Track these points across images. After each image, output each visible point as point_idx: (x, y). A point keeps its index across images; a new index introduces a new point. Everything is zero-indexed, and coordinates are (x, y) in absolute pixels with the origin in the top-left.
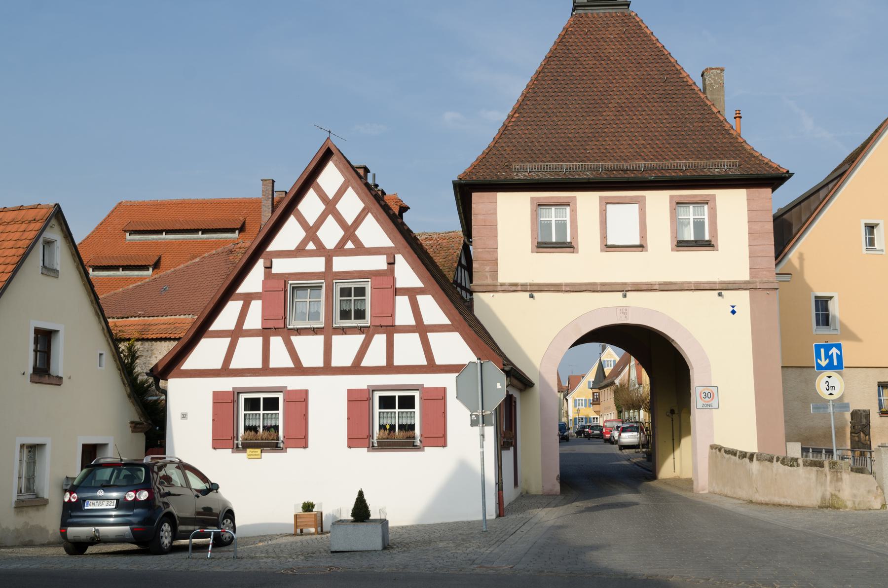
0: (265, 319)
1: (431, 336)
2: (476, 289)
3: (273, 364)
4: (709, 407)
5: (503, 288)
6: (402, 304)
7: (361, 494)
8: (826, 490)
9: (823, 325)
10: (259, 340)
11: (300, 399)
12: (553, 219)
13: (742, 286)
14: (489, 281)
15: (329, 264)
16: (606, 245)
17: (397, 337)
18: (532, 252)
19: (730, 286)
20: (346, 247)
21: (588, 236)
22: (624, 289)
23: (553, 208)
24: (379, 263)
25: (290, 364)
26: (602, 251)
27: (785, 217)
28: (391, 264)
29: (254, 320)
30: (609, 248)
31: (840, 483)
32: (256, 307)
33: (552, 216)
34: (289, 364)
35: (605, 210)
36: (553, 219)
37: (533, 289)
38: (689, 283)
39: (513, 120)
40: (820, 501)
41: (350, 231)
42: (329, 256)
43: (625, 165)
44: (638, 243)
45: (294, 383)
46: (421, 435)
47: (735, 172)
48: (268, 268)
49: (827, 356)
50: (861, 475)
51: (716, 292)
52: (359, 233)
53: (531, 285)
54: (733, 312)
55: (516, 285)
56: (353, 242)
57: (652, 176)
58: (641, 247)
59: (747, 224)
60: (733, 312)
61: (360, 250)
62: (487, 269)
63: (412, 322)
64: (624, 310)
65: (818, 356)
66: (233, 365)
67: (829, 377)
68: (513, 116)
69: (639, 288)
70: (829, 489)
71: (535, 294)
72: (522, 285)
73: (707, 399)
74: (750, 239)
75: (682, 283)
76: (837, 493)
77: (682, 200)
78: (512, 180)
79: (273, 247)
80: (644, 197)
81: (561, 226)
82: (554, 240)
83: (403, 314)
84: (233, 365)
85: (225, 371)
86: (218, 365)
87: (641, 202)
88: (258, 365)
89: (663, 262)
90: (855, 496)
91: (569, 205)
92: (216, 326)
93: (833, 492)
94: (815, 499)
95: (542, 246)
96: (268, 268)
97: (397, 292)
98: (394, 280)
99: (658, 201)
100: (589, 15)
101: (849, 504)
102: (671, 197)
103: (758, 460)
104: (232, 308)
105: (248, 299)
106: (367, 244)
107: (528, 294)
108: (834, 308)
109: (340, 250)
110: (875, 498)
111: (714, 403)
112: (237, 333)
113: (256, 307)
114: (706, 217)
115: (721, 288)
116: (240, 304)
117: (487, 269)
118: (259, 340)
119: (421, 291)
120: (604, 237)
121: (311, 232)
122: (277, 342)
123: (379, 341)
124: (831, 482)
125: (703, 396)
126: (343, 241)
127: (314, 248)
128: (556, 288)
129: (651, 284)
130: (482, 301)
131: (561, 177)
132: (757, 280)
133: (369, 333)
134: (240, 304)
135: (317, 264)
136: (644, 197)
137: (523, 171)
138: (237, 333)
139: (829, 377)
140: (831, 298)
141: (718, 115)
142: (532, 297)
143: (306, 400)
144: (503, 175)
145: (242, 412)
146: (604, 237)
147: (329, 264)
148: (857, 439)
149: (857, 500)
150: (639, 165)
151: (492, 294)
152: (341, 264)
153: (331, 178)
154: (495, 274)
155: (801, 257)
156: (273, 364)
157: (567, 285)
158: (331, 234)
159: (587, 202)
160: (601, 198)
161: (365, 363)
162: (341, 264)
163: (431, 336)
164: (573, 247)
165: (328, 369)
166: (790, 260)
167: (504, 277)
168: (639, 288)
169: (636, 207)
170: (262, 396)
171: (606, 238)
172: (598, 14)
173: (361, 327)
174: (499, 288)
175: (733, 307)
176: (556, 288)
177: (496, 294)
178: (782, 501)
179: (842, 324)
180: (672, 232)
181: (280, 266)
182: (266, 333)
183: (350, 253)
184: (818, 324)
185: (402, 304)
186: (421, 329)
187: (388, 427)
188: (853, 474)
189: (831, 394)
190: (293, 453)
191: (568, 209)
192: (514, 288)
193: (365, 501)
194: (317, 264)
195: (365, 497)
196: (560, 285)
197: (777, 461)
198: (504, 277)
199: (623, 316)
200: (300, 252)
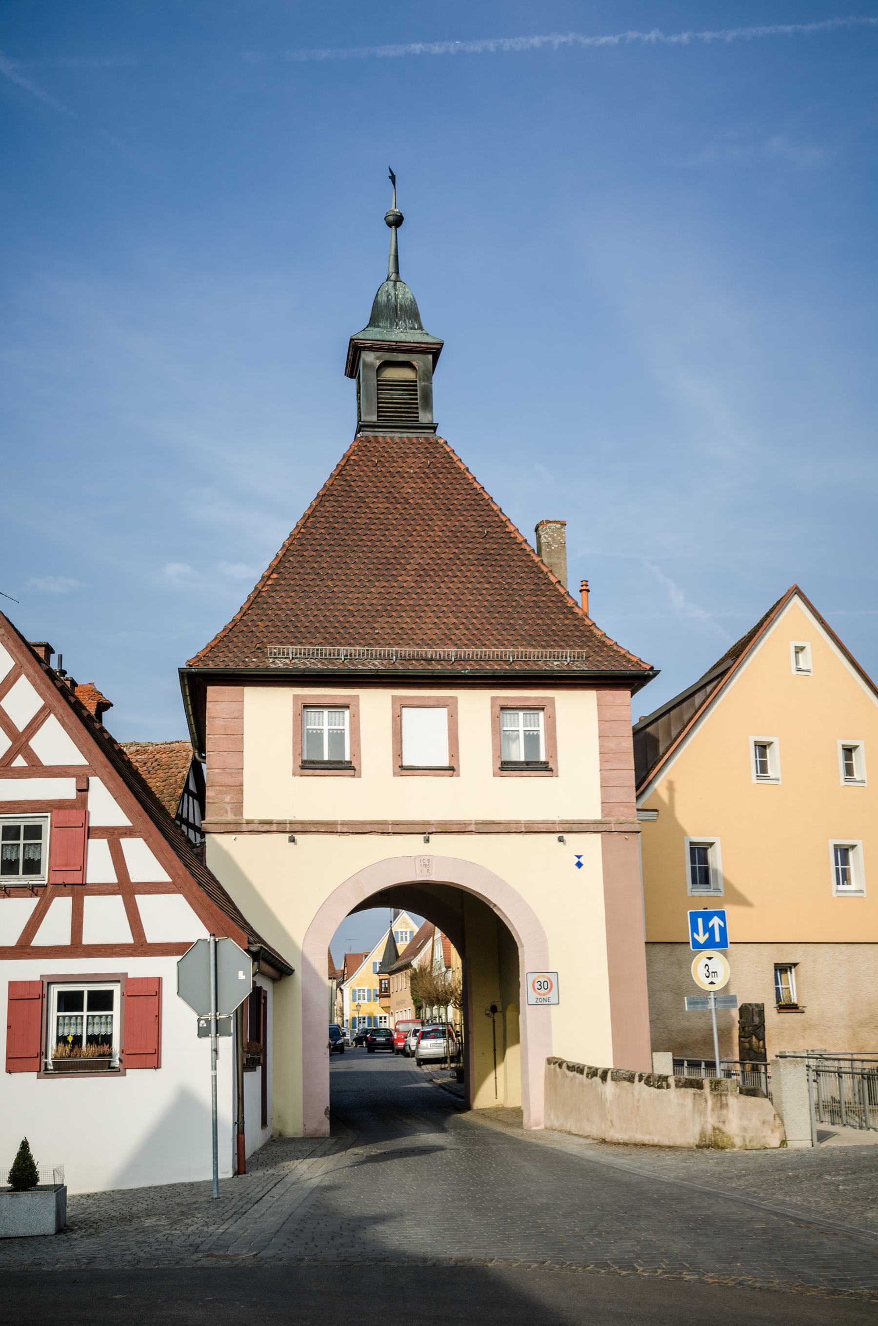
1: (141, 900)
2: (210, 828)
4: (546, 1002)
6: (98, 849)
7: (25, 1146)
8: (706, 1122)
9: (701, 883)
12: (326, 727)
13: (592, 827)
14: (230, 817)
16: (401, 767)
17: (87, 899)
18: (294, 775)
19: (575, 828)
21: (375, 754)
22: (426, 830)
24: (64, 789)
26: (395, 774)
27: (648, 730)
28: (83, 790)
30: (403, 770)
31: (724, 1112)
33: (323, 722)
35: (400, 716)
36: (326, 727)
37: (293, 830)
38: (518, 823)
39: (270, 582)
40: (698, 1137)
43: (429, 652)
44: (445, 763)
46: (122, 1051)
47: (581, 667)
49: (711, 931)
50: (753, 1099)
54: (579, 865)
55: (270, 823)
56: (24, 757)
57: (466, 669)
58: (451, 769)
59: (597, 740)
61: (36, 769)
62: (228, 798)
64: (426, 862)
67: (710, 958)
68: (269, 578)
69: (447, 829)
70: (711, 1121)
71: (297, 837)
72: (279, 823)
73: (543, 991)
74: (603, 761)
75: (509, 823)
76: (721, 1125)
78: (267, 669)
80: (455, 699)
81: (337, 738)
82: (326, 758)
83: (99, 866)
87: (451, 705)
90: (745, 1129)
91: (347, 707)
93: (716, 1125)
94: (691, 1137)
95: (309, 766)
97: (91, 833)
98: (87, 814)
99: (475, 704)
100: (380, 439)
101: (738, 1141)
102: (493, 699)
103: (613, 1079)
106: (46, 761)
107: (287, 836)
108: (716, 859)
110: (773, 1131)
111: (553, 996)
115: (563, 830)
117: (228, 798)
119: (128, 832)
120: (398, 754)
123: (61, 906)
124: (713, 1110)
125: (537, 986)
128: (328, 828)
130: (219, 847)
131: (336, 667)
132: (612, 819)
133: (44, 895)
136: (455, 699)
137: (284, 656)
139: (710, 958)
140: (711, 844)
141: (557, 586)
142: (292, 840)
144: (253, 663)
146: (398, 754)
148: (747, 1045)
149: (749, 1136)
150: (448, 654)
151: (233, 836)
154: (238, 806)
155: (671, 787)
157: (344, 823)
159: (375, 703)
160: (394, 698)
161: (37, 942)
164: (353, 769)
166: (656, 791)
167: (251, 812)
168: (447, 829)
169: (445, 711)
170: (86, 988)
171: (400, 755)
172: (392, 438)
173: (33, 886)
174: (245, 828)
175: (579, 857)
176: (328, 828)
177: (240, 837)
178: (646, 1139)
179: (726, 882)
180: (494, 750)
183: (20, 773)
184: (694, 881)
185: (98, 849)
186: (126, 889)
187: (70, 1039)
188: (743, 1098)
189: (712, 983)
191: (347, 713)
192: (266, 827)
193: (30, 1157)
195: (32, 1152)
196: (334, 823)
197: (640, 1080)
198: (251, 812)
199: (425, 869)
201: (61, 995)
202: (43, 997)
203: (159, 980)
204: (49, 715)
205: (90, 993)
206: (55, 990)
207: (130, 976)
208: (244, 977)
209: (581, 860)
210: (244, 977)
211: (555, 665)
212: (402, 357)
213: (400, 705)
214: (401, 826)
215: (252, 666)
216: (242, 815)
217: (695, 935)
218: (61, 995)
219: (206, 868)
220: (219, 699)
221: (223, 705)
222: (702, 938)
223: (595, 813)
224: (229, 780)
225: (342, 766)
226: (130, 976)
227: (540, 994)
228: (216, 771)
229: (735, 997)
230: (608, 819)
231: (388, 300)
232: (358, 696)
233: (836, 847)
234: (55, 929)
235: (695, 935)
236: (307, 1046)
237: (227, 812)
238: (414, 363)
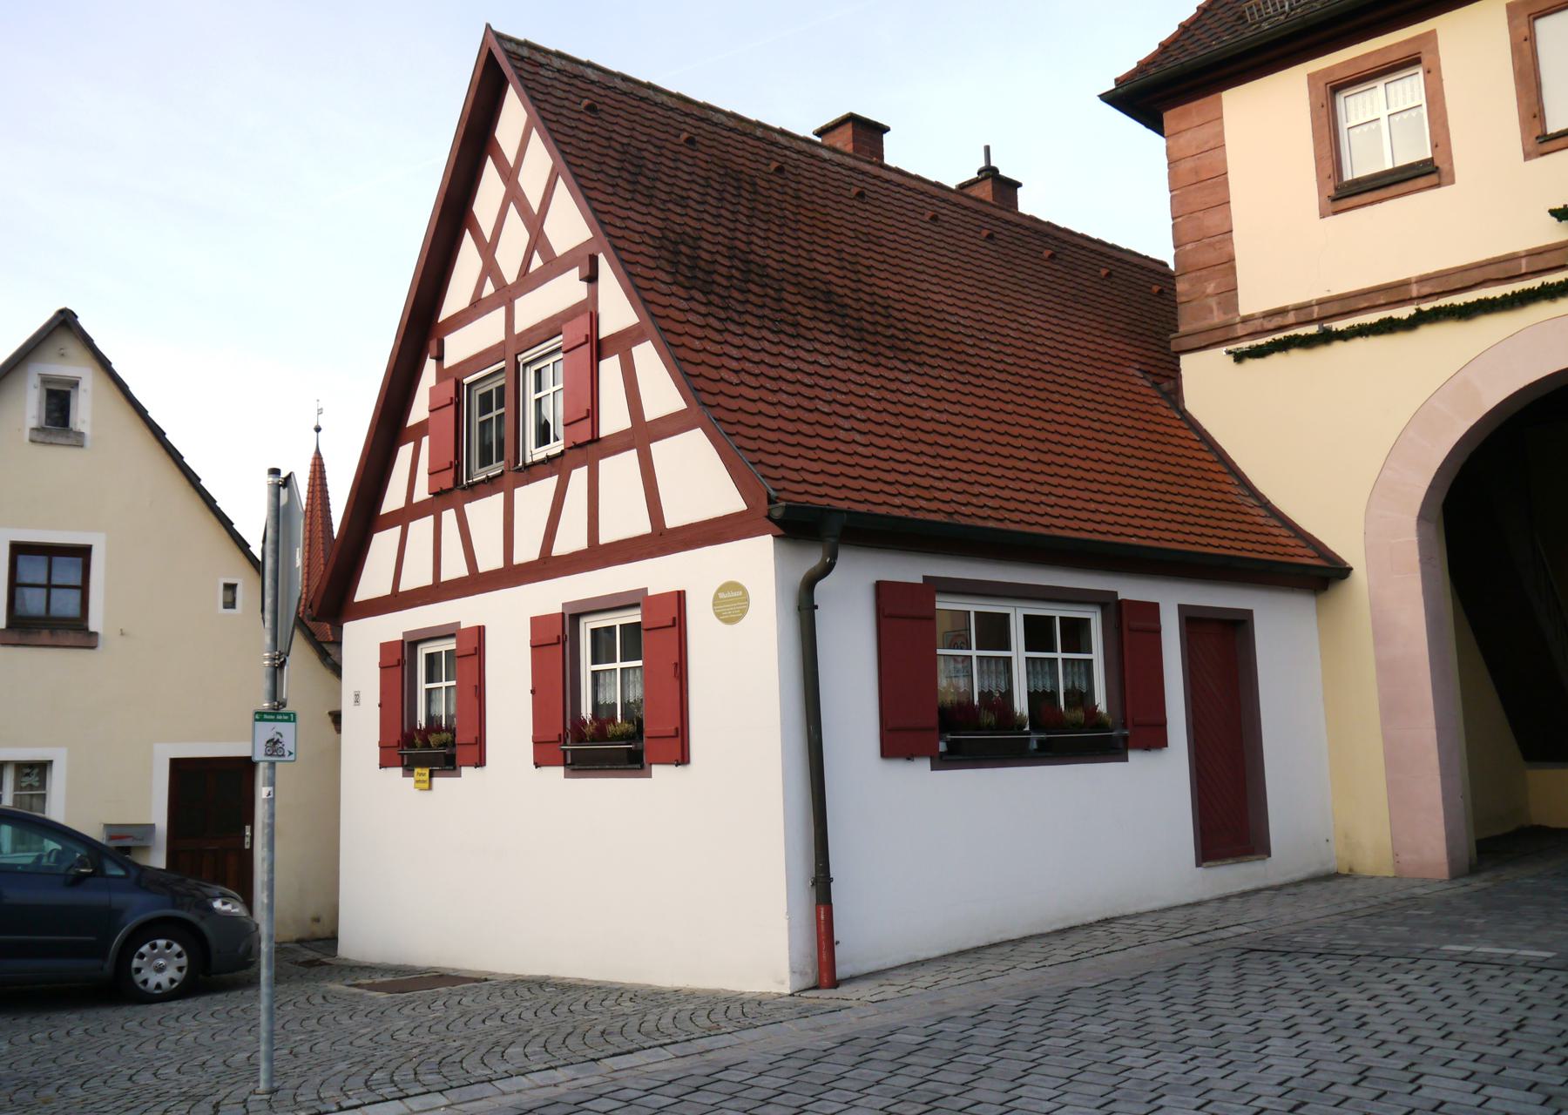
14: (1217, 318)
16: (1545, 138)
23: (1380, 84)
35: (1531, 38)
53: (1321, 302)
62: (1211, 288)
72: (1298, 308)
95: (1346, 194)
97: (599, 349)
109: (528, 281)
117: (1211, 288)
143: (479, 651)
153: (513, 116)
154: (1230, 293)
157: (1423, 280)
200: (478, 307)
201: (1086, 623)
203: (680, 596)
206: (588, 625)
207: (650, 593)
214: (1547, 256)
216: (1236, 309)
218: (1086, 623)
220: (1183, 126)
221: (1189, 135)
224: (1210, 257)
226: (650, 593)
229: (189, 777)
232: (1433, 33)
236: (1391, 709)
237: (1211, 311)
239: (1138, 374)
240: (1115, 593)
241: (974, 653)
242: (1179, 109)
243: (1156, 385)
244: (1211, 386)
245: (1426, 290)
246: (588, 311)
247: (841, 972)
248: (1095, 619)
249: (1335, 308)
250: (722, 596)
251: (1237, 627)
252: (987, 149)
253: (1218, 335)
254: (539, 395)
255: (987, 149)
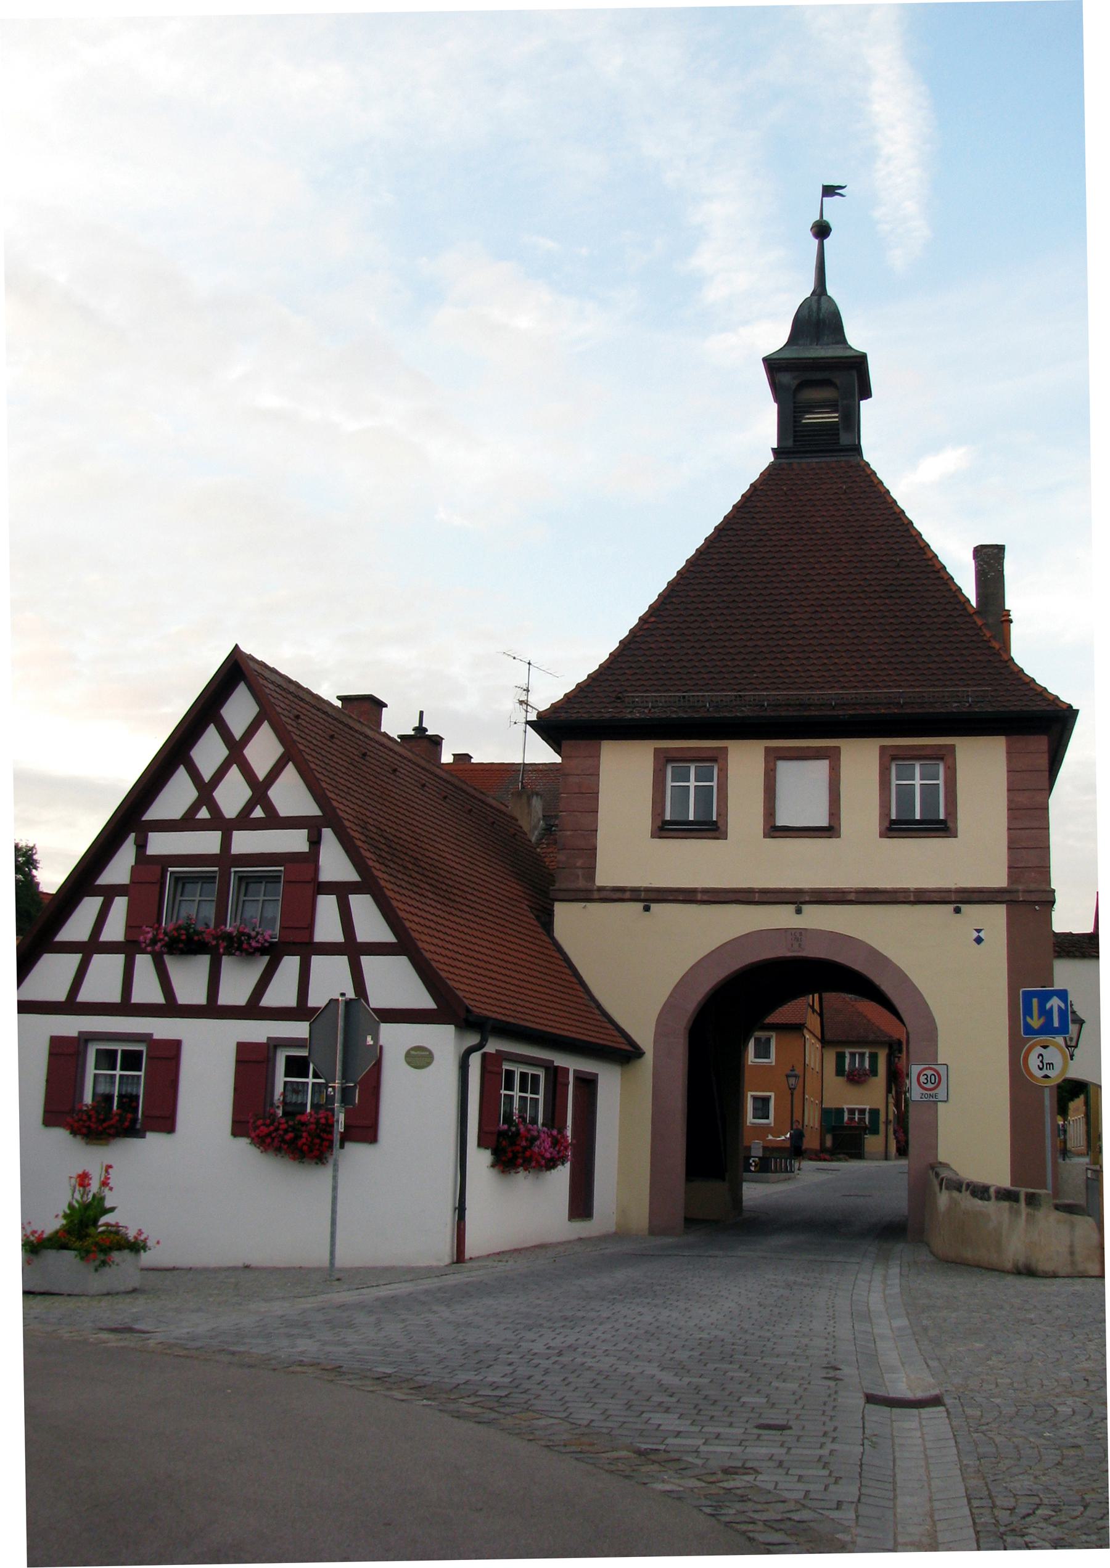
0: (129, 927)
1: (365, 960)
3: (137, 998)
5: (603, 895)
6: (327, 907)
10: (119, 959)
11: (168, 1055)
14: (581, 884)
15: (226, 842)
17: (316, 961)
19: (975, 897)
20: (199, 816)
24: (295, 841)
25: (159, 998)
28: (315, 842)
29: (115, 930)
30: (774, 831)
32: (120, 904)
34: (159, 998)
35: (774, 770)
41: (260, 790)
42: (226, 827)
44: (824, 822)
45: (162, 1028)
48: (141, 846)
51: (951, 907)
52: (272, 793)
54: (979, 940)
58: (830, 831)
60: (979, 940)
61: (274, 821)
63: (338, 937)
64: (798, 935)
65: (1028, 1011)
66: (83, 996)
67: (1045, 1047)
74: (1011, 818)
77: (675, 754)
79: (154, 813)
81: (929, 793)
83: (327, 926)
84: (83, 996)
85: (71, 1006)
86: (61, 996)
87: (833, 756)
88: (115, 997)
89: (864, 855)
92: (66, 934)
96: (141, 846)
98: (316, 869)
99: (861, 758)
104: (90, 906)
105: (110, 893)
106: (283, 812)
109: (244, 821)
112: (91, 947)
113: (120, 904)
114: (941, 782)
116: (98, 901)
118: (119, 959)
120: (770, 811)
121: (206, 790)
122: (144, 963)
123: (290, 965)
125: (923, 1079)
126: (249, 807)
127: (208, 816)
129: (843, 892)
132: (1020, 887)
133: (274, 953)
134: (98, 901)
135: (208, 842)
138: (91, 947)
144: (608, 713)
145: (91, 1070)
146: (770, 811)
147: (226, 842)
152: (245, 842)
154: (590, 870)
156: (137, 998)
158: (232, 795)
159: (745, 761)
160: (883, 749)
162: (245, 842)
163: (365, 960)
165: (212, 1010)
167: (605, 877)
169: (823, 765)
170: (120, 1047)
175: (978, 931)
181: (160, 844)
182: (129, 948)
185: (327, 905)
186: (352, 949)
190: (154, 1140)
194: (208, 842)
196: (694, 891)
198: (605, 877)
200: (187, 823)
201: (538, 1076)
202: (81, 1056)
204: (287, 763)
205: (123, 1051)
208: (371, 1043)
209: (982, 934)
210: (371, 1043)
211: (954, 707)
212: (818, 376)
213: (773, 758)
215: (607, 716)
217: (1028, 1019)
219: (553, 938)
222: (1036, 1023)
223: (999, 879)
225: (710, 828)
227: (926, 1089)
228: (569, 833)
230: (1015, 887)
231: (810, 316)
232: (726, 748)
233: (766, 835)
234: (282, 991)
235: (1028, 1019)
238: (837, 381)
239: (526, 908)
240: (152, 1035)
241: (118, 1072)
242: (572, 742)
243: (538, 917)
244: (569, 921)
245: (705, 898)
246: (311, 858)
247: (467, 1255)
248: (541, 1073)
249: (653, 896)
250: (413, 1052)
251: (587, 1085)
252: (421, 713)
253: (581, 895)
254: (1022, 1198)
255: (421, 713)
